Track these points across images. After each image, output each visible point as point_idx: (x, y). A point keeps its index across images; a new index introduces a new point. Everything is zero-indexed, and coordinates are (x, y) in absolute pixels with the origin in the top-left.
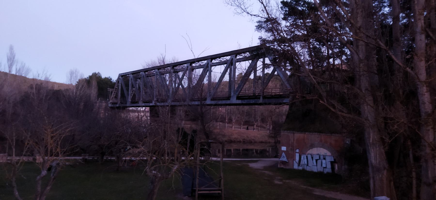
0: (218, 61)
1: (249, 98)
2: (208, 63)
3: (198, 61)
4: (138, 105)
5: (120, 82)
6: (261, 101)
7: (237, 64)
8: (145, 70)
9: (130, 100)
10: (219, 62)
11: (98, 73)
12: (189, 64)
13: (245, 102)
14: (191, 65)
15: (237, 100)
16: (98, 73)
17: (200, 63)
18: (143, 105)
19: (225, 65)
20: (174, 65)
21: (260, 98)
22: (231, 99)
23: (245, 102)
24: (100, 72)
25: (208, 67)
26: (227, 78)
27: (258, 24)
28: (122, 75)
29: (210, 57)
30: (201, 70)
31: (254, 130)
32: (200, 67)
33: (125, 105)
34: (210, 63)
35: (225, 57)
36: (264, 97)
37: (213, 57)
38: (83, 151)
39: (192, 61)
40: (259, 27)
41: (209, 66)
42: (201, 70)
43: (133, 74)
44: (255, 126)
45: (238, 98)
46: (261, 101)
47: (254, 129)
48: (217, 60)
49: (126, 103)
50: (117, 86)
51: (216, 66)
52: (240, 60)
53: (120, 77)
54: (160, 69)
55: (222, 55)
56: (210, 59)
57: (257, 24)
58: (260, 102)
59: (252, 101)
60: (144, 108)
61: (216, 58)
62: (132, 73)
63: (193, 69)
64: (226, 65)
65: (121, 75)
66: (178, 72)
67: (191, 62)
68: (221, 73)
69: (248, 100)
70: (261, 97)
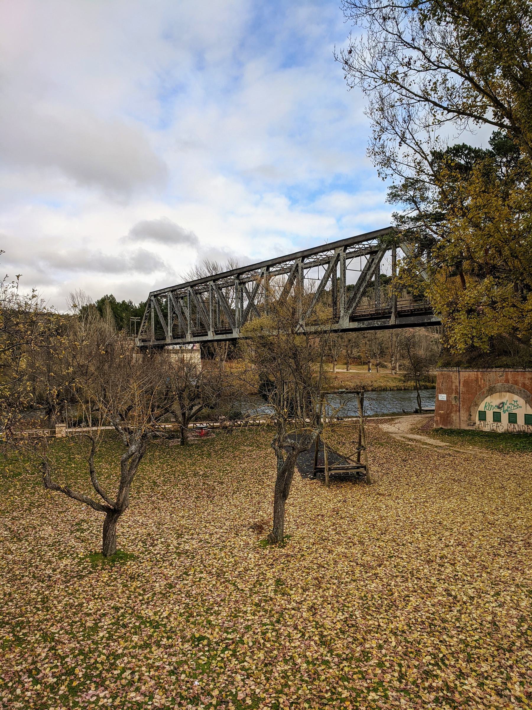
0: (312, 260)
1: (372, 317)
2: (297, 264)
3: (280, 263)
4: (184, 340)
5: (152, 306)
6: (392, 321)
7: (305, 271)
8: (192, 284)
9: (170, 334)
10: (314, 261)
11: (111, 296)
12: (265, 268)
13: (365, 324)
14: (268, 269)
15: (350, 323)
16: (111, 296)
17: (282, 265)
18: (192, 340)
19: (326, 266)
20: (238, 273)
21: (390, 317)
22: (341, 321)
23: (365, 324)
24: (114, 295)
25: (298, 270)
26: (329, 286)
27: (390, 191)
28: (155, 293)
29: (300, 255)
30: (286, 277)
31: (369, 371)
32: (282, 272)
33: (162, 342)
34: (300, 265)
35: (325, 253)
36: (400, 314)
37: (306, 254)
38: (124, 501)
39: (270, 263)
40: (394, 196)
41: (300, 270)
42: (286, 277)
43: (172, 291)
44: (371, 364)
45: (353, 319)
46: (392, 321)
47: (369, 369)
48: (312, 258)
49: (164, 339)
50: (148, 313)
51: (310, 267)
52: (351, 256)
53: (152, 298)
54: (195, 285)
55: (322, 249)
56: (300, 257)
57: (389, 191)
58: (390, 324)
59: (377, 323)
60: (191, 345)
61: (275, 264)
62: (171, 289)
63: (270, 275)
64: (327, 265)
65: (153, 294)
66: (244, 283)
67: (269, 264)
68: (361, 271)
69: (370, 321)
70: (393, 316)
